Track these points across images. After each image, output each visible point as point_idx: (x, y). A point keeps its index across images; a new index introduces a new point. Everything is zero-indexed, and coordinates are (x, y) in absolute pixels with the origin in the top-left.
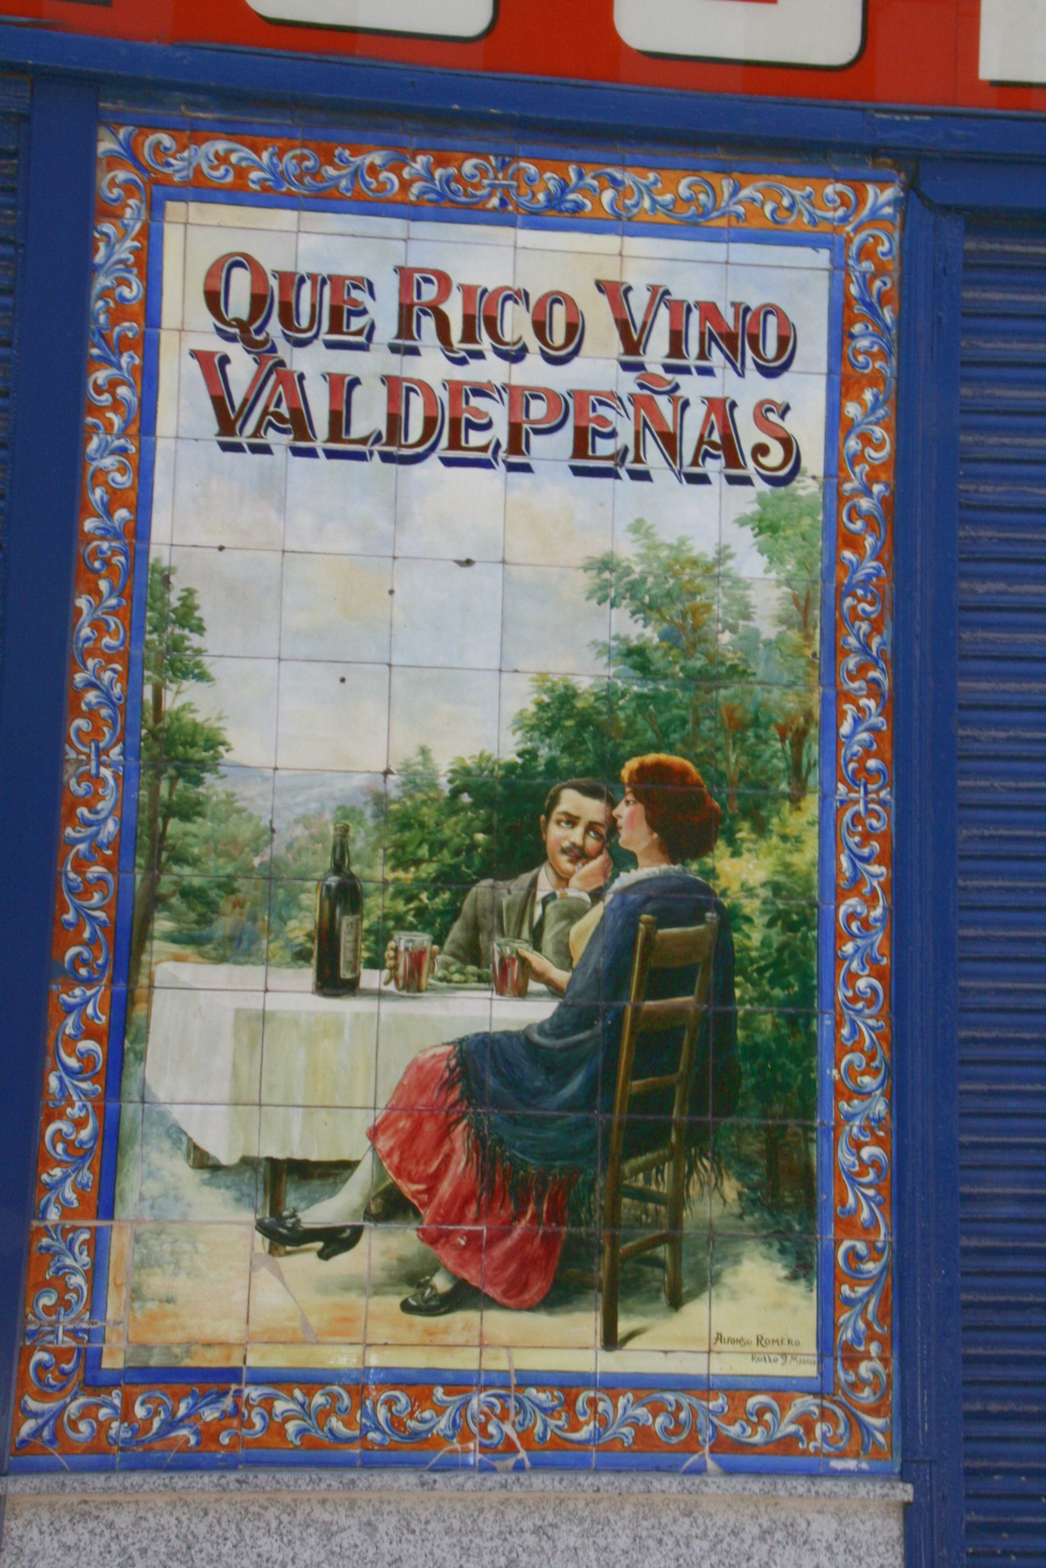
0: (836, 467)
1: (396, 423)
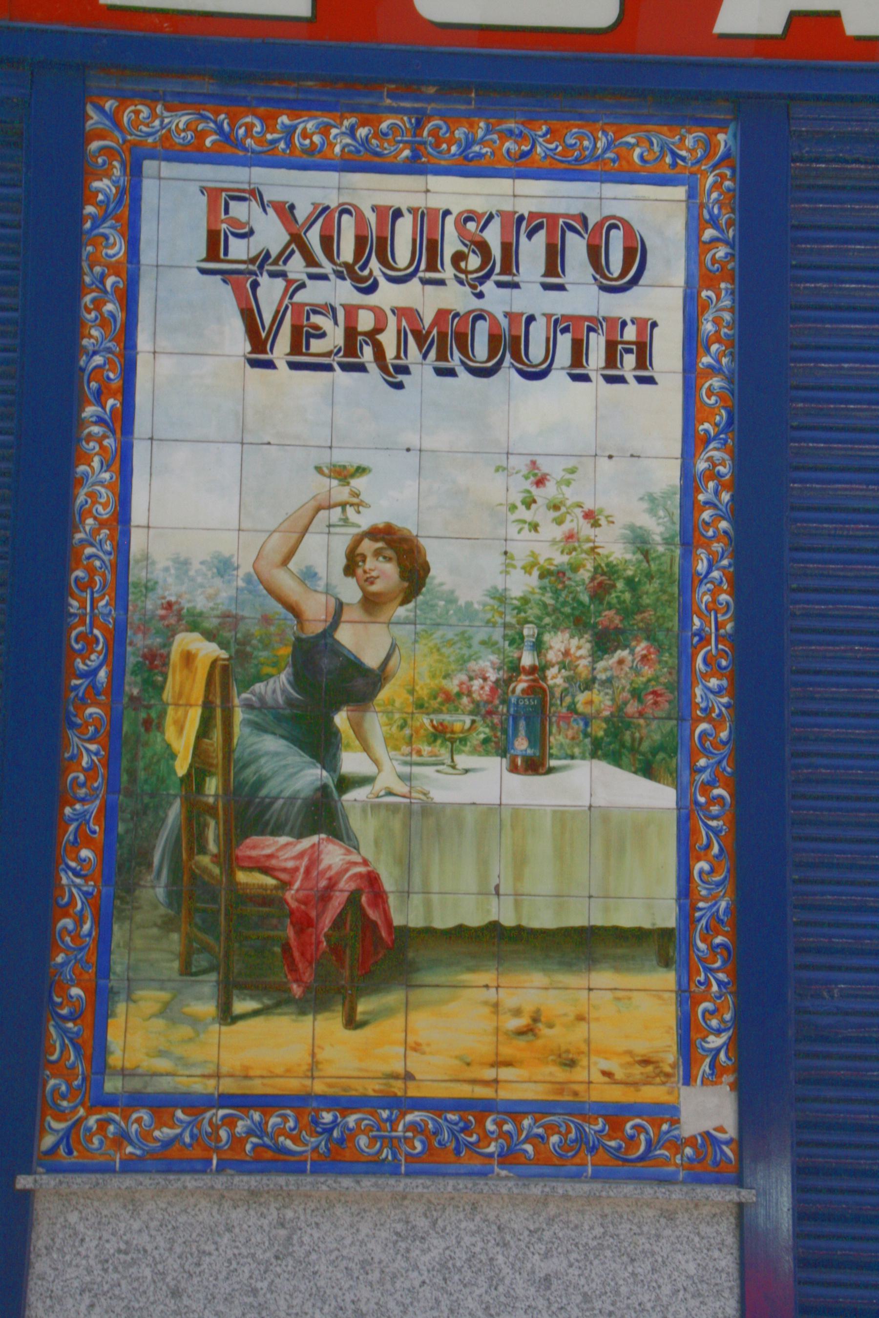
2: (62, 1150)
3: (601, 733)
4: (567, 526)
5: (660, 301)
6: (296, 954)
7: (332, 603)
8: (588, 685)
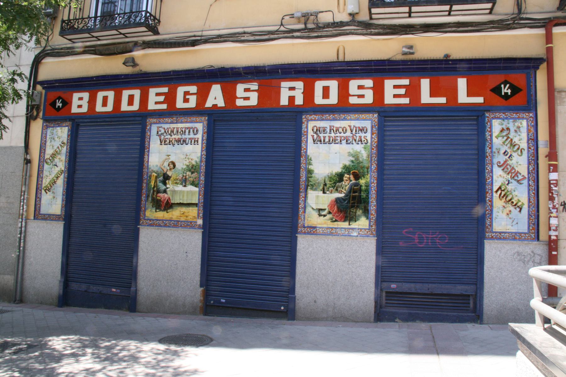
0: (372, 142)
1: (329, 140)
5: (199, 136)
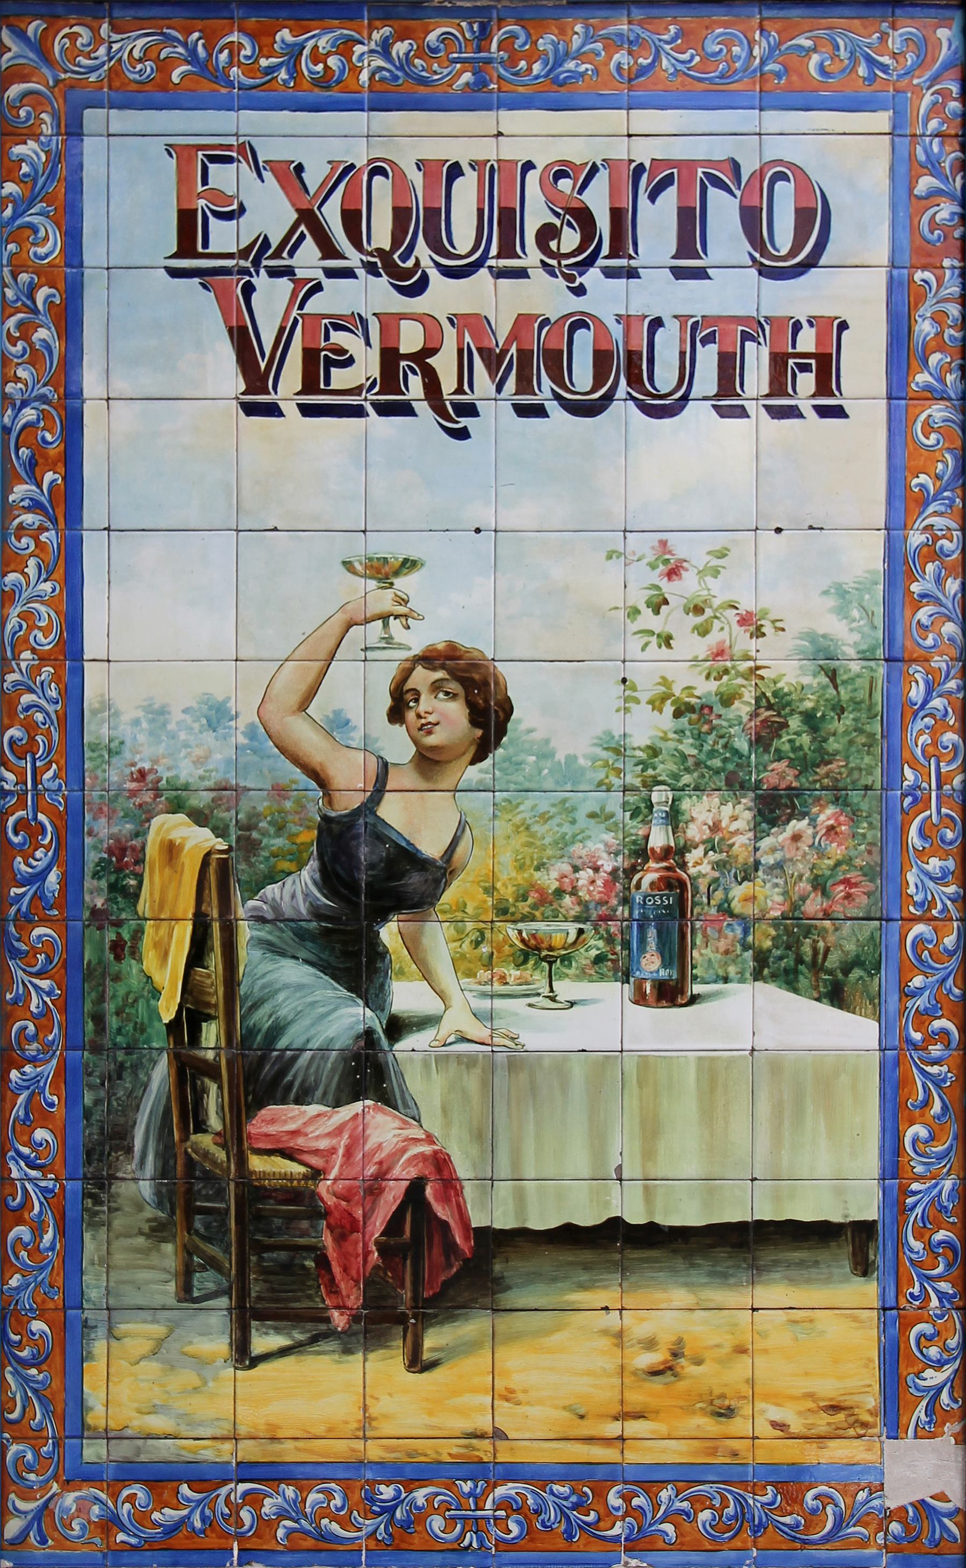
2: (33, 1538)
3: (768, 943)
4: (714, 638)
5: (852, 291)
6: (336, 1270)
7: (373, 763)
8: (748, 873)
